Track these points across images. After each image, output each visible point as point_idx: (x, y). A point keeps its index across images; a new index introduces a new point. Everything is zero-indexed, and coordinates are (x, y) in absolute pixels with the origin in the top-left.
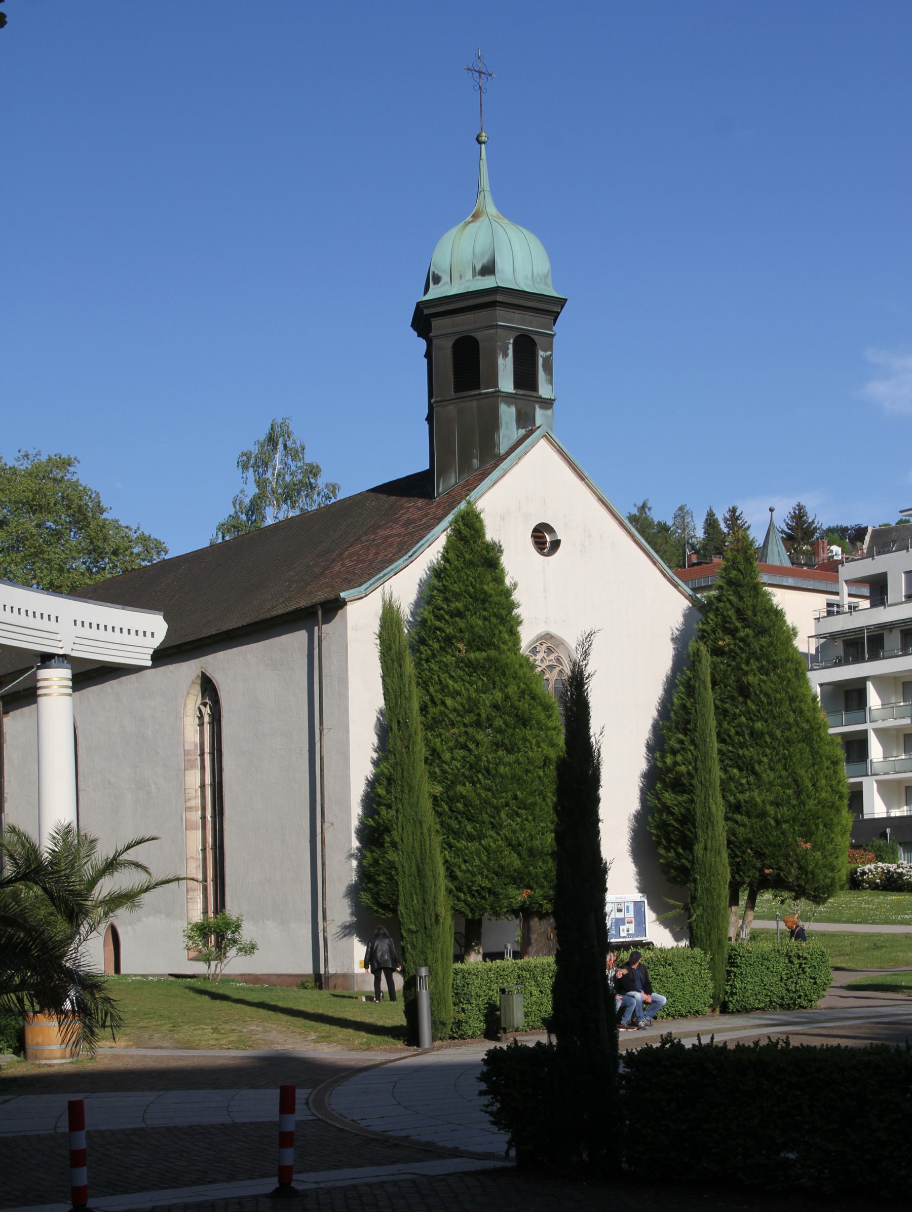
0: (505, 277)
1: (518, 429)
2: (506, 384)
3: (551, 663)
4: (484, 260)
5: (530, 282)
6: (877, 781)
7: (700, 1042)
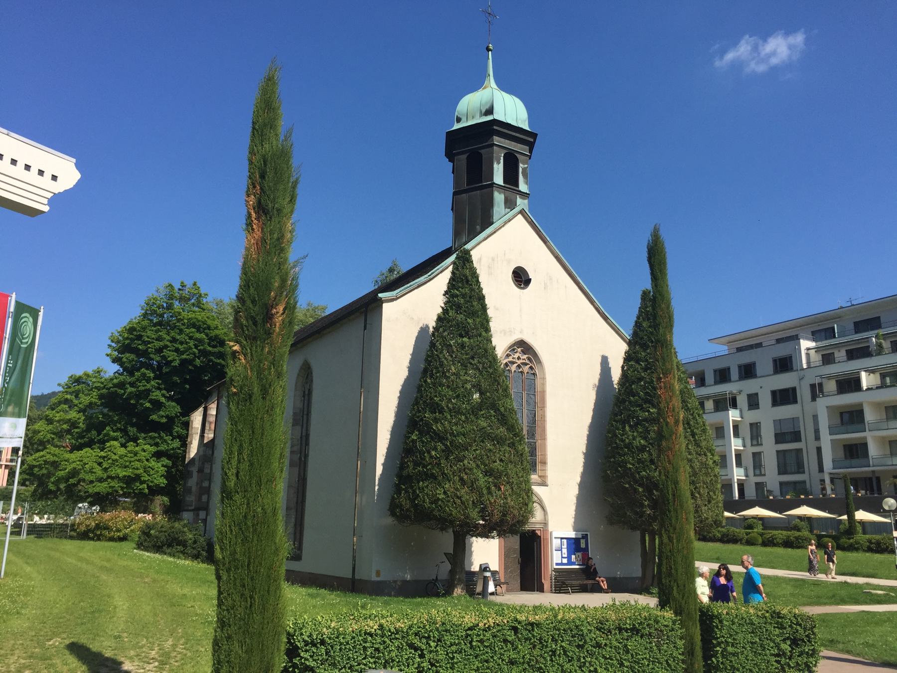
0: (498, 115)
1: (505, 208)
2: (498, 178)
3: (524, 361)
4: (487, 107)
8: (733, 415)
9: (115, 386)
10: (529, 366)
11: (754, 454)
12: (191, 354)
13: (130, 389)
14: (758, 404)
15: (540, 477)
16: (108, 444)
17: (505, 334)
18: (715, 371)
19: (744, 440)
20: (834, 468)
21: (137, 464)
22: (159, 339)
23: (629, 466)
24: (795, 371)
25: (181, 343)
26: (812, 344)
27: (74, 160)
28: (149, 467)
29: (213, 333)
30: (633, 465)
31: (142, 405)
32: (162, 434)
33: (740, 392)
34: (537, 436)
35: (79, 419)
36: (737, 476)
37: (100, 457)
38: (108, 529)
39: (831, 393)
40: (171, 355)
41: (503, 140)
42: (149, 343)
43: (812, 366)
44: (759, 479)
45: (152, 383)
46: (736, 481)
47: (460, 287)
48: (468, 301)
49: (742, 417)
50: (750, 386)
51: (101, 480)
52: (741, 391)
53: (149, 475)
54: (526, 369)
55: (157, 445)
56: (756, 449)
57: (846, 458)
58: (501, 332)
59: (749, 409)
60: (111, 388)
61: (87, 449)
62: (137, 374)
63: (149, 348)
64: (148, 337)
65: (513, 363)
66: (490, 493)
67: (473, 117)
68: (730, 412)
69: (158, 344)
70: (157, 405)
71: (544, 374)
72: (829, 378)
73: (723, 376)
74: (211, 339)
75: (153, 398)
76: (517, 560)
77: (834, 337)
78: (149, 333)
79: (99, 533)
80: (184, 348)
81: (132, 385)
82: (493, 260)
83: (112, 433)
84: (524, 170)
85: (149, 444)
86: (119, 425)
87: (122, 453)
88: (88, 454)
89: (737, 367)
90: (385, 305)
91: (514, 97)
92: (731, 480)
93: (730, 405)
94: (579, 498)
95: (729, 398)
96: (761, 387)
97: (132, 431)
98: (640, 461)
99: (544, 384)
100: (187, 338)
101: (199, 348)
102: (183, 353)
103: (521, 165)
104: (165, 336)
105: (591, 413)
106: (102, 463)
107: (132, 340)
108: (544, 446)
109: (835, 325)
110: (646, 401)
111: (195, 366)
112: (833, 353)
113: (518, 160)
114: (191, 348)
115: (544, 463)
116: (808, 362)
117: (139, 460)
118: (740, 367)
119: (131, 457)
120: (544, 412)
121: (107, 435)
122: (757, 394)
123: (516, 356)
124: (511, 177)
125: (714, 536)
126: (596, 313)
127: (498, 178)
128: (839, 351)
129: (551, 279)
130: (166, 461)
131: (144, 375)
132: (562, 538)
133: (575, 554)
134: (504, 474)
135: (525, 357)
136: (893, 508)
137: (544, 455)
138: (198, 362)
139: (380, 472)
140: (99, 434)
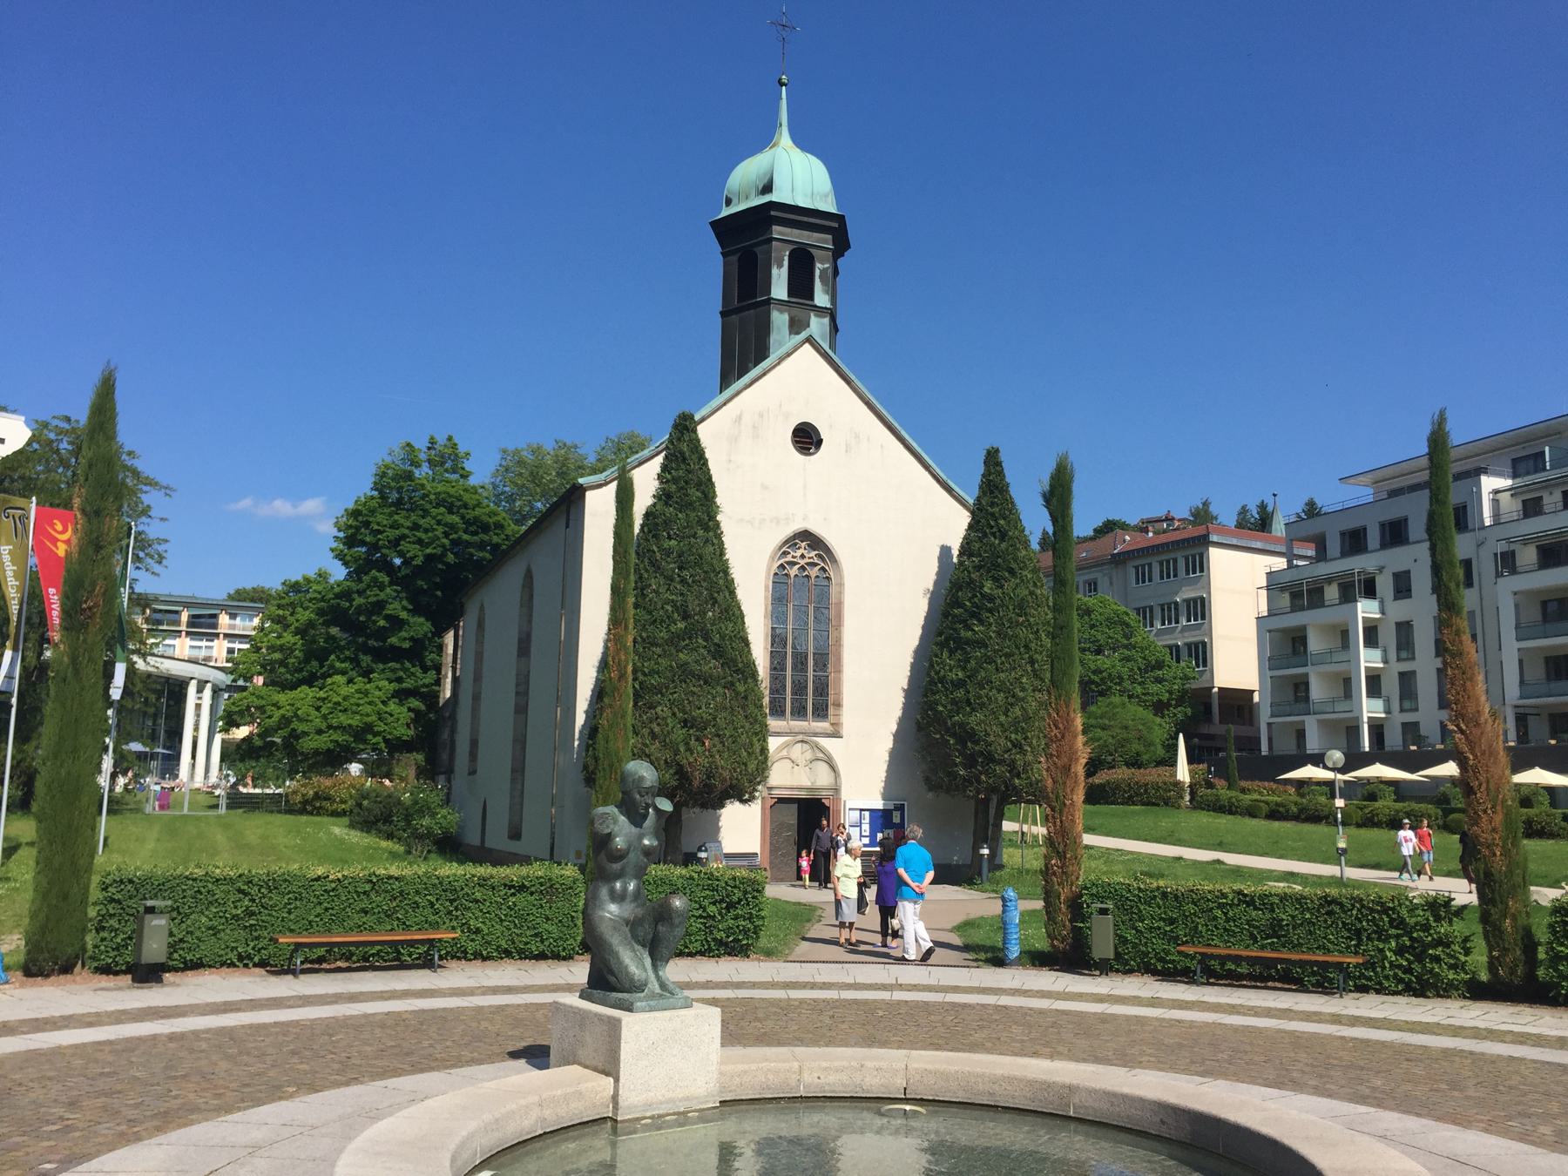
2: (780, 290)
5: (809, 200)
6: (1318, 721)
7: (483, 841)
8: (1366, 609)
9: (337, 596)
10: (819, 567)
11: (1402, 675)
12: (439, 546)
13: (359, 601)
14: (1410, 590)
15: (832, 724)
16: (329, 681)
17: (778, 522)
18: (1343, 534)
19: (1385, 651)
20: (1521, 697)
21: (368, 709)
22: (395, 526)
23: (941, 709)
24: (1471, 531)
25: (426, 531)
26: (1505, 483)
27: (23, 418)
28: (386, 712)
29: (470, 514)
30: (945, 707)
31: (375, 622)
32: (408, 665)
33: (1381, 569)
34: (830, 667)
35: (295, 644)
36: (1368, 712)
37: (319, 699)
38: (330, 799)
39: (1527, 568)
40: (412, 549)
41: (788, 230)
42: (379, 532)
43: (1502, 521)
44: (1409, 717)
45: (388, 590)
46: (1365, 720)
47: (672, 469)
48: (682, 488)
49: (1383, 613)
50: (1398, 558)
51: (320, 732)
52: (1383, 568)
53: (385, 724)
54: (814, 572)
55: (399, 680)
56: (1406, 667)
57: (1549, 678)
58: (771, 521)
59: (1396, 598)
60: (330, 599)
61: (304, 688)
62: (366, 578)
63: (380, 539)
64: (378, 524)
65: (793, 564)
66: (689, 750)
67: (747, 198)
68: (1359, 604)
69: (392, 534)
70: (397, 623)
71: (841, 577)
72: (1525, 542)
73: (1355, 542)
74: (468, 522)
75: (389, 612)
76: (792, 840)
77: (1544, 469)
78: (380, 518)
79: (318, 805)
80: (429, 538)
81: (360, 593)
82: (761, 415)
83: (338, 665)
84: (823, 272)
85: (388, 679)
86: (347, 653)
87: (346, 694)
88: (302, 695)
89: (1378, 525)
90: (589, 494)
91: (809, 155)
92: (1358, 719)
93: (1360, 593)
94: (895, 755)
95: (1359, 581)
96: (1415, 561)
97: (366, 660)
98: (954, 702)
99: (841, 593)
100: (433, 522)
101: (451, 537)
102: (428, 545)
103: (818, 265)
104: (402, 521)
105: (919, 632)
106: (321, 707)
107: (357, 529)
108: (839, 681)
109: (1547, 449)
110: (973, 615)
111: (448, 565)
112: (1541, 498)
113: (813, 257)
114: (438, 539)
115: (838, 705)
116: (1496, 514)
117: (370, 703)
118: (1382, 525)
119: (359, 699)
120: (840, 633)
121: (332, 666)
122: (1408, 572)
123: (798, 553)
124: (801, 286)
125: (1287, 811)
126: (934, 482)
127: (780, 290)
128: (1551, 493)
129: (857, 437)
130: (415, 703)
131: (375, 579)
132: (861, 810)
133: (882, 832)
134: (712, 723)
135: (813, 554)
136: (1340, 766)
137: (839, 694)
138: (451, 558)
139: (582, 723)
140: (322, 666)
